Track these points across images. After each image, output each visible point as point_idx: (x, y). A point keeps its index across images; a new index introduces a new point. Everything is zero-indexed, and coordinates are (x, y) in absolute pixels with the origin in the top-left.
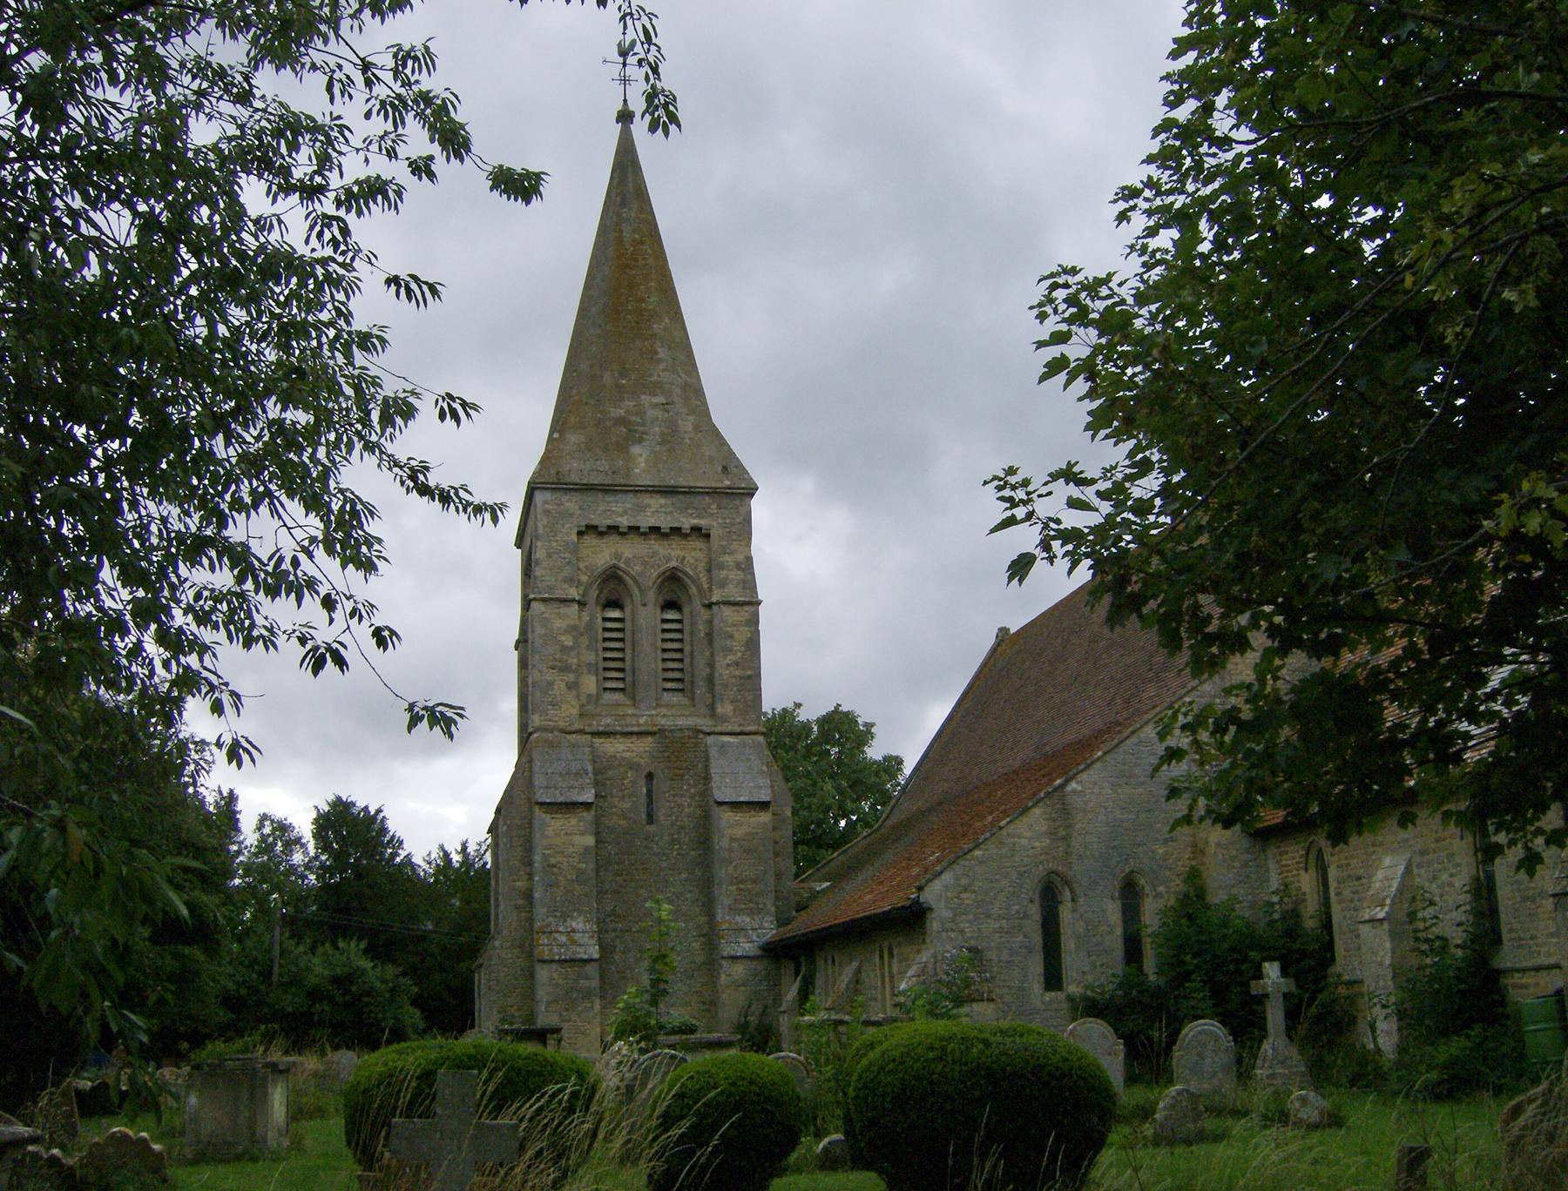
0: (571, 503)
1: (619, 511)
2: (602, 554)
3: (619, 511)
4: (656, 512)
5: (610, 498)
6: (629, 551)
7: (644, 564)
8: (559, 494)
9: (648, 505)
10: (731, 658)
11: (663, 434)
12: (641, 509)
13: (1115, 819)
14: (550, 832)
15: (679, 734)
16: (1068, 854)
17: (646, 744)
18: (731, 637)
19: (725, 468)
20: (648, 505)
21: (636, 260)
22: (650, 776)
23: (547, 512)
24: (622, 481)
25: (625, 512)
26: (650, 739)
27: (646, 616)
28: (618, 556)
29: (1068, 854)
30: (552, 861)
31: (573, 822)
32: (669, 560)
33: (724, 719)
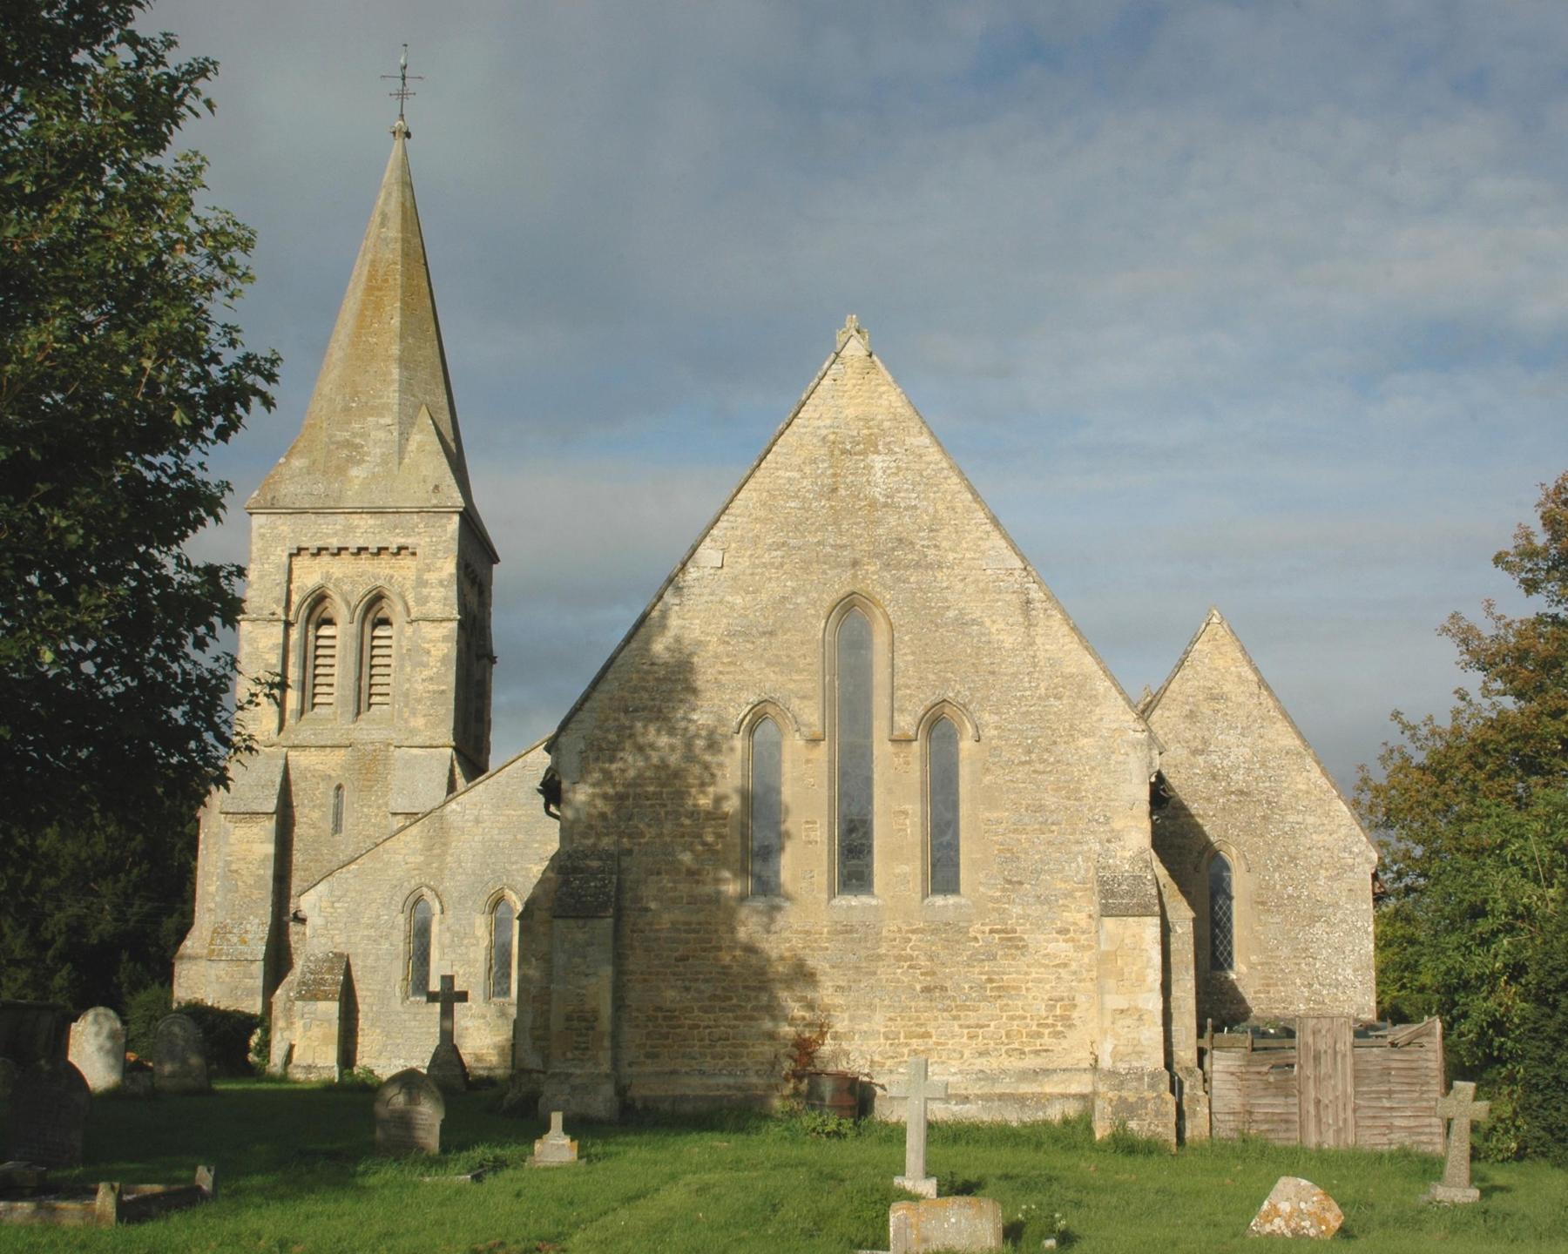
0: (284, 525)
1: (330, 531)
2: (309, 576)
3: (330, 531)
4: (366, 531)
5: (321, 519)
6: (339, 568)
7: (353, 583)
8: (273, 517)
9: (358, 526)
10: (426, 673)
11: (383, 454)
12: (350, 529)
13: (492, 839)
14: (232, 839)
15: (371, 747)
16: (440, 870)
17: (340, 756)
18: (428, 652)
19: (436, 487)
20: (358, 526)
21: (386, 281)
22: (339, 787)
23: (262, 536)
24: (332, 504)
25: (335, 534)
26: (343, 751)
27: (342, 633)
28: (328, 576)
29: (440, 870)
30: (234, 867)
31: (255, 830)
32: (377, 578)
33: (413, 732)
